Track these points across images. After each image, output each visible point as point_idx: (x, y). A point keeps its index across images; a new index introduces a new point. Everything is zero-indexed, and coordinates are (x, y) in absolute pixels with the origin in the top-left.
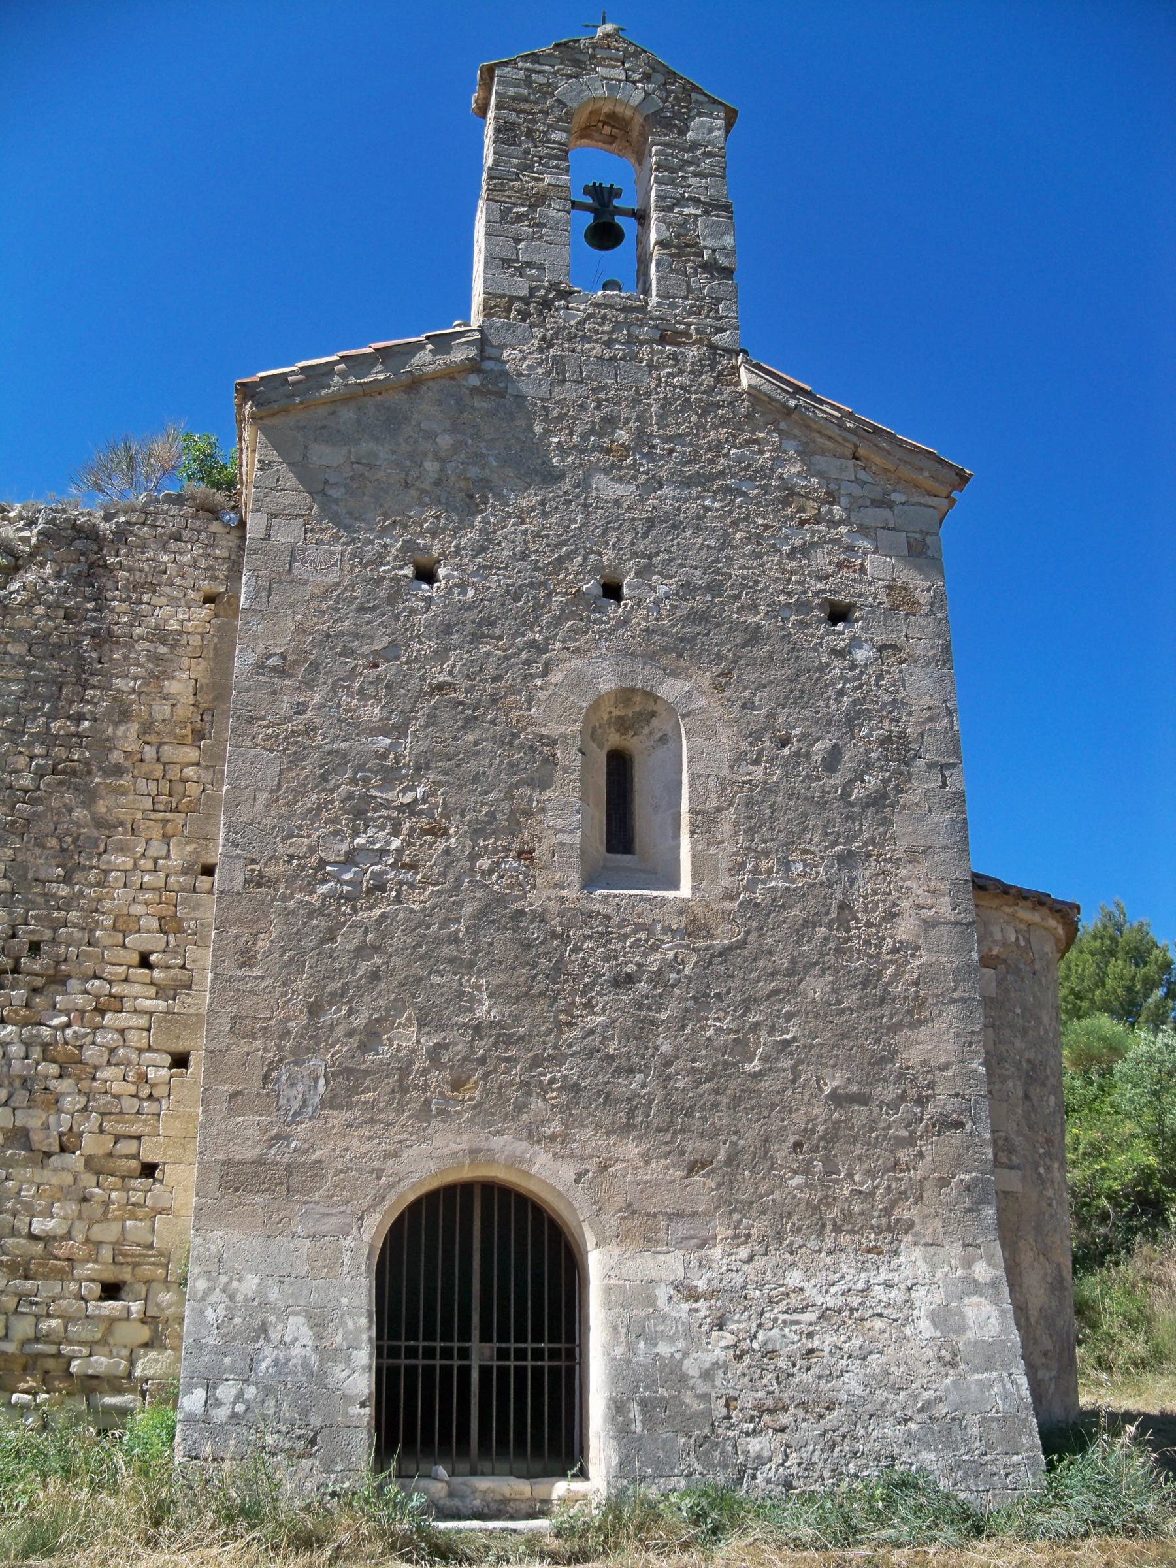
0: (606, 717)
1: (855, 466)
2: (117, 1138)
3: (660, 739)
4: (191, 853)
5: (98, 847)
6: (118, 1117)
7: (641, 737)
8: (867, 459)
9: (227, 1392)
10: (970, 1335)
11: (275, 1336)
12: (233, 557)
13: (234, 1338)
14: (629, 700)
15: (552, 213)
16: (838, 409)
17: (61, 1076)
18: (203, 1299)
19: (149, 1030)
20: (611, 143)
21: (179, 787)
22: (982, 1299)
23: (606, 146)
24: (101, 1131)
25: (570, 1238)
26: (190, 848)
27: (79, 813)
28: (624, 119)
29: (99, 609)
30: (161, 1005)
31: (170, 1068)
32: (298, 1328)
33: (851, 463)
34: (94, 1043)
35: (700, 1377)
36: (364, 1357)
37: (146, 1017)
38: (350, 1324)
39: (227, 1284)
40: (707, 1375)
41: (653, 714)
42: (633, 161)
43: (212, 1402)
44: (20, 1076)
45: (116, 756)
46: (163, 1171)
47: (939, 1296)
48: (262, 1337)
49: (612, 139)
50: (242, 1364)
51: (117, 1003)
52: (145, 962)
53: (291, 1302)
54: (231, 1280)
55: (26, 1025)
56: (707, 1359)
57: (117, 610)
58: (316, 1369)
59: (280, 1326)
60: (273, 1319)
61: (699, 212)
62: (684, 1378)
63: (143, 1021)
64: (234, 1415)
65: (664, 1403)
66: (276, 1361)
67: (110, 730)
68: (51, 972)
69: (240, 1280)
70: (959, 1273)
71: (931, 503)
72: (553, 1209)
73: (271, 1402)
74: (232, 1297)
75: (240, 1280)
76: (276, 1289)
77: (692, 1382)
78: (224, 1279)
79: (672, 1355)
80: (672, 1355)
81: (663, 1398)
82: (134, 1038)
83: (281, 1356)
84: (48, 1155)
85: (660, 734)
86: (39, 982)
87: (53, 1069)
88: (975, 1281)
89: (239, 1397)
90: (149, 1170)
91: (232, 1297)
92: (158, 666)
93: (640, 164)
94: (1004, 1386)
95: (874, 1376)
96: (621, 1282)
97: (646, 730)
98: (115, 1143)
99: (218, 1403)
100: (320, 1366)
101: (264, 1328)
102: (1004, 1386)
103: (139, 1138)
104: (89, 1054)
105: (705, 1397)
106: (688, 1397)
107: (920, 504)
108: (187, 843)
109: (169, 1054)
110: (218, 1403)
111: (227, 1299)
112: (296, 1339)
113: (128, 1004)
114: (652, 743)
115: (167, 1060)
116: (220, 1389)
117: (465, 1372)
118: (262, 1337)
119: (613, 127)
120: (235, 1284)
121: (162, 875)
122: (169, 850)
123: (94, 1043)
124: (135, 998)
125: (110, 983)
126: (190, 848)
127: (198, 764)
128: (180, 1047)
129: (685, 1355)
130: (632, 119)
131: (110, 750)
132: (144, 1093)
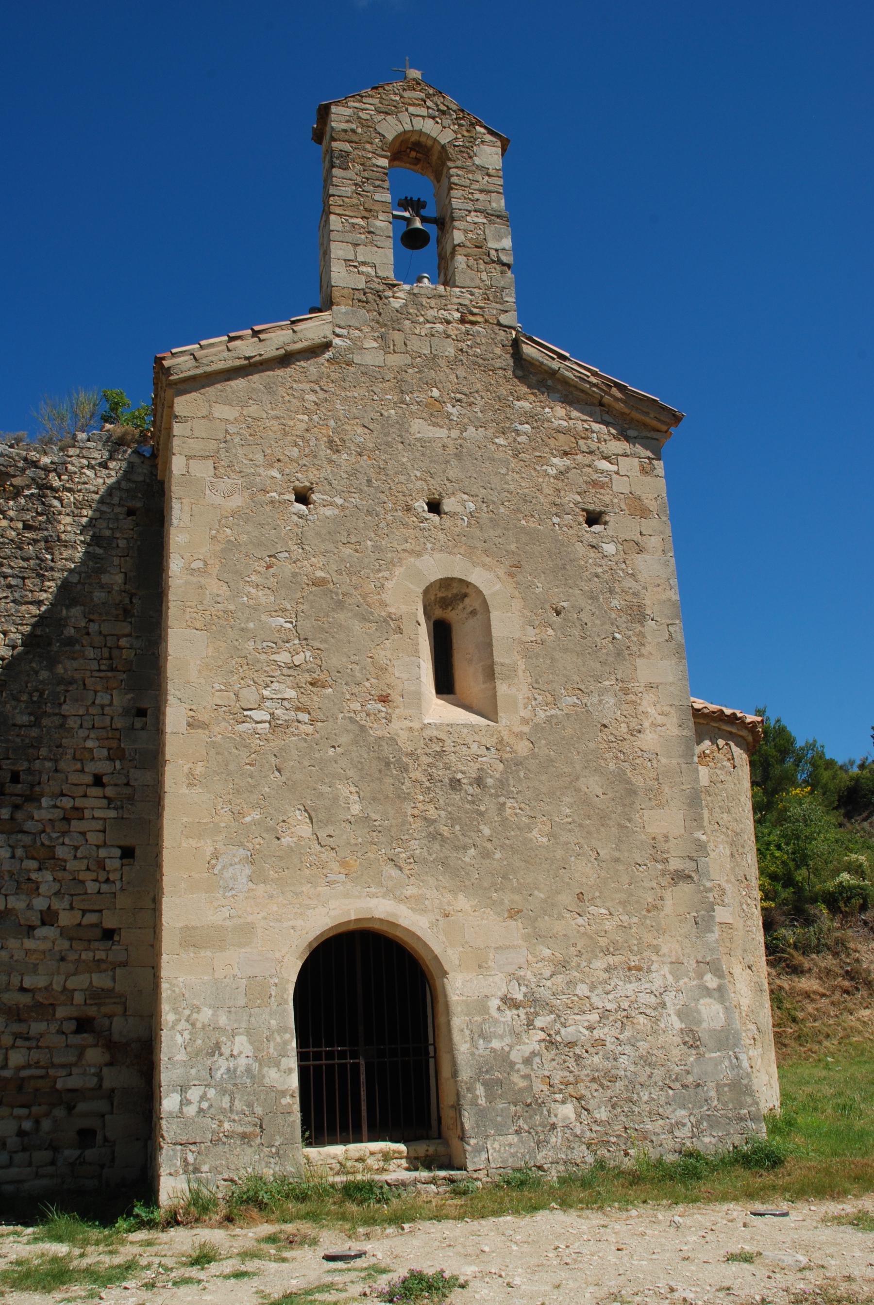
0: (433, 598)
1: (601, 411)
2: (84, 912)
3: (471, 612)
4: (129, 700)
5: (59, 699)
6: (84, 897)
7: (457, 611)
8: (609, 406)
9: (194, 1094)
10: (704, 1025)
11: (226, 1051)
12: (148, 481)
13: (197, 1055)
14: (449, 585)
15: (378, 223)
16: (588, 370)
17: (40, 869)
18: (173, 1028)
19: (104, 831)
20: (416, 164)
21: (115, 652)
22: (711, 1000)
23: (412, 167)
24: (72, 908)
25: (424, 968)
26: (130, 696)
27: (44, 675)
28: (426, 146)
29: (48, 521)
30: (112, 814)
31: (121, 858)
32: (241, 1044)
33: (598, 409)
34: (63, 844)
35: (523, 1062)
36: (292, 1062)
37: (101, 822)
38: (278, 1039)
39: (189, 1016)
40: (527, 1061)
41: (465, 595)
42: (432, 178)
43: (185, 1102)
44: (9, 871)
45: (70, 631)
46: (120, 935)
47: (682, 999)
48: (217, 1052)
49: (417, 161)
50: (205, 1074)
51: (78, 812)
52: (98, 781)
53: (236, 1026)
54: (192, 1013)
55: (13, 833)
56: (527, 1050)
57: (63, 522)
58: (256, 1072)
59: (229, 1044)
60: (224, 1039)
61: (485, 221)
62: (512, 1064)
63: (99, 825)
64: (201, 1110)
65: (500, 1083)
66: (228, 1070)
67: (64, 612)
68: (28, 792)
69: (198, 1012)
70: (695, 983)
71: (655, 437)
72: (413, 949)
73: (226, 1099)
74: (193, 1025)
75: (198, 1012)
76: (224, 1017)
77: (517, 1066)
78: (187, 1012)
79: (502, 1049)
80: (502, 1049)
81: (498, 1079)
82: (92, 838)
83: (231, 1065)
84: (32, 928)
85: (471, 609)
86: (19, 801)
87: (33, 864)
88: (707, 988)
89: (203, 1098)
90: (109, 935)
91: (193, 1025)
92: (96, 563)
93: (438, 181)
94: (730, 1061)
95: (641, 1057)
96: (464, 998)
97: (461, 606)
98: (83, 916)
99: (189, 1103)
100: (260, 1070)
101: (218, 1046)
102: (730, 1061)
103: (100, 911)
104: (60, 852)
105: (527, 1077)
106: (515, 1078)
107: (648, 438)
108: (126, 694)
109: (119, 847)
110: (189, 1103)
111: (190, 1027)
112: (241, 1053)
113: (87, 814)
114: (465, 615)
115: (118, 852)
116: (190, 1092)
117: (356, 1066)
118: (217, 1052)
119: (417, 152)
120: (195, 1016)
121: (108, 719)
122: (112, 699)
123: (63, 844)
124: (93, 809)
125: (74, 798)
126: (130, 696)
127: (129, 635)
128: (127, 842)
129: (511, 1047)
130: (432, 146)
131: (65, 626)
132: (102, 876)
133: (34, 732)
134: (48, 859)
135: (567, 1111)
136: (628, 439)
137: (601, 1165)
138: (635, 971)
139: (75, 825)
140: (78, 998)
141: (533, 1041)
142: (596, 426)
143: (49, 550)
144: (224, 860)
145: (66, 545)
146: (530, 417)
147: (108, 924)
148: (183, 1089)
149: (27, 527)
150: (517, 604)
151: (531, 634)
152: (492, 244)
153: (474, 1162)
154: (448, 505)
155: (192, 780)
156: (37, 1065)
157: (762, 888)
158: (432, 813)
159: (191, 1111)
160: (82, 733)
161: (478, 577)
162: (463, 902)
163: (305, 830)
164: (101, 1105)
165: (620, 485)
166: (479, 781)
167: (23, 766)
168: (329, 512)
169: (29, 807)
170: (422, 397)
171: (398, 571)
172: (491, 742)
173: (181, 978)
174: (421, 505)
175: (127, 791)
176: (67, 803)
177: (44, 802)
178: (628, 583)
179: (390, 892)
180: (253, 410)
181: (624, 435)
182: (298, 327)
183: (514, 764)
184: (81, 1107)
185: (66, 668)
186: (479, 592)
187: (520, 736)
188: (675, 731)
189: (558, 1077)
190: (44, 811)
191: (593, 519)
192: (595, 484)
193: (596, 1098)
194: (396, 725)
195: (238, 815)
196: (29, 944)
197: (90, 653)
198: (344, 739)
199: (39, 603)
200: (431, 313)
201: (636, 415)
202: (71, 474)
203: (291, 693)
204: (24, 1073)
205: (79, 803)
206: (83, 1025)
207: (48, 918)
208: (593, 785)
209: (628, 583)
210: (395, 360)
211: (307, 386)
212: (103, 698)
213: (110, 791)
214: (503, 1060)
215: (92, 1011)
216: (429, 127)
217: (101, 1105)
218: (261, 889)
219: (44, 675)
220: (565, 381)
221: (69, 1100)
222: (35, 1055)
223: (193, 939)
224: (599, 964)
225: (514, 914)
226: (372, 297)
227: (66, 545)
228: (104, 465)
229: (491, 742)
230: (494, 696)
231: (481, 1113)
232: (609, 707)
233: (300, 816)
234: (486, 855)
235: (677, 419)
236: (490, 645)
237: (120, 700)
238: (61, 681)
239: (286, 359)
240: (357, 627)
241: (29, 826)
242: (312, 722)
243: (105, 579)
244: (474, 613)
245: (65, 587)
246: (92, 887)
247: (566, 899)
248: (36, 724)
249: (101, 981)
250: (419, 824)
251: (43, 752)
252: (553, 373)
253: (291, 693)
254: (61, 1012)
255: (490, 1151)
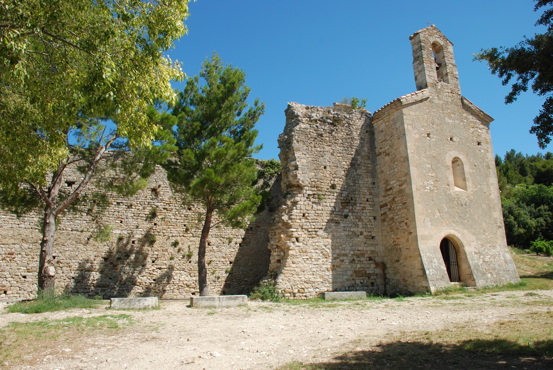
27: (355, 173)
30: (371, 208)
43: (430, 272)
45: (359, 162)
90: (373, 237)
104: (363, 217)
133: (354, 188)
134: (360, 219)
135: (489, 275)
136: (483, 124)
137: (497, 286)
138: (494, 247)
139: (365, 211)
140: (369, 252)
141: (481, 262)
142: (478, 121)
143: (352, 140)
144: (426, 220)
145: (355, 140)
146: (466, 118)
147: (373, 235)
148: (429, 269)
149: (347, 134)
150: (468, 164)
151: (471, 171)
152: (454, 73)
153: (478, 285)
154: (454, 139)
155: (419, 203)
156: (363, 268)
157: (110, 252)
158: (459, 211)
159: (431, 274)
160: (364, 188)
161: (461, 157)
162: (465, 231)
163: (438, 214)
164: (375, 277)
165: (483, 136)
166: (466, 205)
167: (353, 196)
168: (434, 140)
169: (355, 206)
170: (446, 112)
171: (448, 155)
172: (467, 195)
173: (422, 246)
174: (449, 139)
175: (373, 203)
176: (362, 205)
177: (358, 205)
178: (486, 160)
179: (454, 229)
180: (417, 113)
181: (482, 124)
182: (424, 93)
183: (471, 201)
184: (372, 277)
185: (359, 171)
186: (461, 160)
187: (471, 194)
188: (497, 194)
189: (487, 268)
190: (358, 207)
191: (479, 144)
192: (478, 135)
193: (494, 273)
194: (451, 191)
195: (427, 210)
196: (359, 239)
197: (363, 168)
198: (443, 194)
199: (352, 155)
200: (446, 90)
201: (485, 119)
202: (354, 121)
203: (432, 183)
204: (360, 269)
205: (365, 205)
206: (370, 259)
207: (361, 233)
208: (484, 206)
209: (486, 160)
210: (441, 102)
211: (426, 108)
212: (366, 180)
213: (370, 203)
214: (477, 264)
215: (371, 256)
216: (439, 40)
217: (375, 277)
218: (433, 227)
219: (355, 173)
220: (472, 109)
221: (369, 276)
222: (362, 265)
223: (424, 238)
224: (488, 245)
225: (474, 234)
226: (434, 85)
227: (355, 140)
228: (360, 119)
229: (467, 195)
230: (466, 185)
231: (477, 275)
232: (485, 188)
233: (437, 211)
234: (468, 221)
235: (493, 120)
236: (464, 173)
237: (370, 180)
238: (358, 175)
239: (421, 101)
240: (442, 167)
241: (355, 211)
242: (437, 190)
243: (364, 149)
244: (459, 165)
245: (357, 151)
246: (369, 226)
247: (482, 231)
248: (355, 186)
249: (372, 248)
250: (457, 214)
251: (357, 193)
252: (470, 107)
253: (432, 183)
254: (366, 256)
255: (480, 283)
